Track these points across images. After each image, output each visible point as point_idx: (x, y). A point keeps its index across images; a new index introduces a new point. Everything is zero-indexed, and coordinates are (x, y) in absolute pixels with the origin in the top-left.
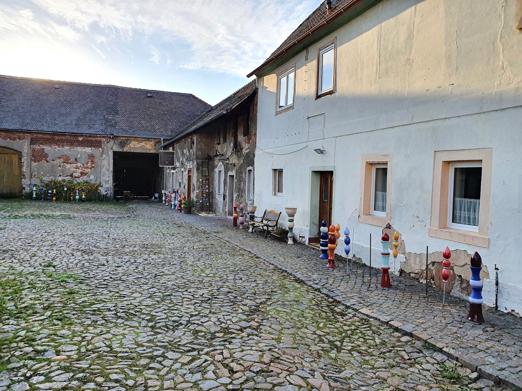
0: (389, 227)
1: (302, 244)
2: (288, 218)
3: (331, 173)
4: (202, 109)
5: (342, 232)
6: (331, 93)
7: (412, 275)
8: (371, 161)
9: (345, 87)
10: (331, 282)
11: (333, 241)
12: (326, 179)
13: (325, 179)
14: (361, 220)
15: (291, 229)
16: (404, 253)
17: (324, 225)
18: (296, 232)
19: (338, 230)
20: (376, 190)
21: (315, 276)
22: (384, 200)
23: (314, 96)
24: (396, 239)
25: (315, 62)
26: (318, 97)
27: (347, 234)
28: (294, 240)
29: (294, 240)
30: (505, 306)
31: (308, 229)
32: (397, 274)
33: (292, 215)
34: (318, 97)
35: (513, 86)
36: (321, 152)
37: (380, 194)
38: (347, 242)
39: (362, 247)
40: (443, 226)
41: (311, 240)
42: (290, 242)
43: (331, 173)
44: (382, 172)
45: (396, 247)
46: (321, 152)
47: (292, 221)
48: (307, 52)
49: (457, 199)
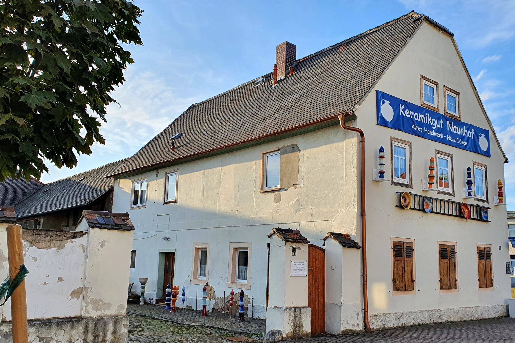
0: (207, 284)
1: (152, 304)
2: (141, 286)
3: (173, 254)
4: (32, 186)
5: (181, 292)
6: (174, 202)
7: (219, 310)
8: (198, 246)
9: (183, 200)
10: (174, 317)
11: (175, 296)
12: (170, 258)
13: (168, 259)
14: (192, 282)
15: (143, 294)
16: (215, 299)
17: (168, 287)
18: (146, 296)
19: (178, 289)
20: (201, 264)
21: (165, 316)
22: (205, 270)
23: (163, 202)
24: (211, 290)
25: (163, 180)
26: (165, 203)
27: (183, 290)
28: (145, 303)
29: (145, 303)
30: (256, 316)
31: (156, 293)
32: (211, 311)
33: (144, 282)
34: (165, 203)
35: (258, 216)
36: (167, 239)
37: (203, 266)
38: (184, 295)
39: (192, 299)
40: (234, 281)
41: (157, 301)
42: (142, 303)
43: (173, 254)
44: (204, 253)
45: (210, 294)
46: (167, 239)
47: (144, 288)
48: (158, 172)
49: (240, 267)
